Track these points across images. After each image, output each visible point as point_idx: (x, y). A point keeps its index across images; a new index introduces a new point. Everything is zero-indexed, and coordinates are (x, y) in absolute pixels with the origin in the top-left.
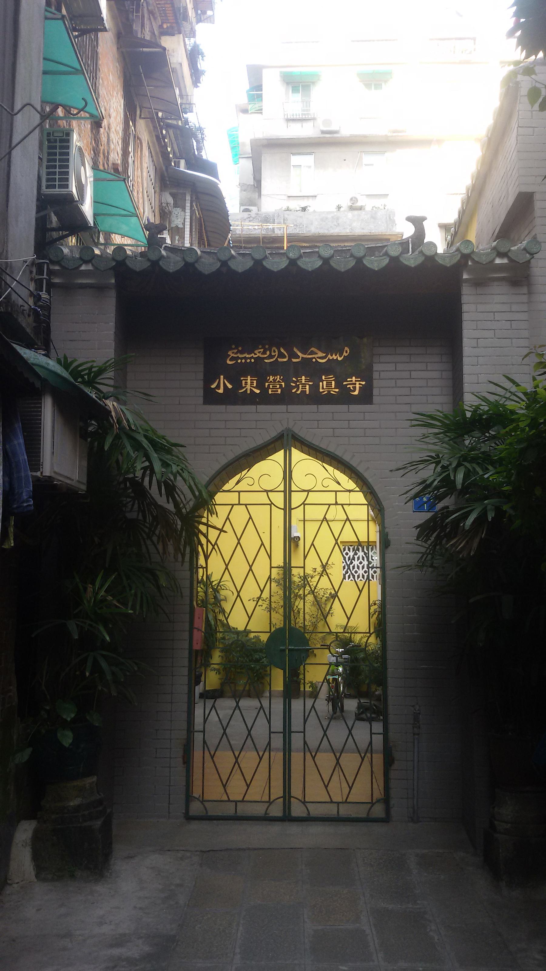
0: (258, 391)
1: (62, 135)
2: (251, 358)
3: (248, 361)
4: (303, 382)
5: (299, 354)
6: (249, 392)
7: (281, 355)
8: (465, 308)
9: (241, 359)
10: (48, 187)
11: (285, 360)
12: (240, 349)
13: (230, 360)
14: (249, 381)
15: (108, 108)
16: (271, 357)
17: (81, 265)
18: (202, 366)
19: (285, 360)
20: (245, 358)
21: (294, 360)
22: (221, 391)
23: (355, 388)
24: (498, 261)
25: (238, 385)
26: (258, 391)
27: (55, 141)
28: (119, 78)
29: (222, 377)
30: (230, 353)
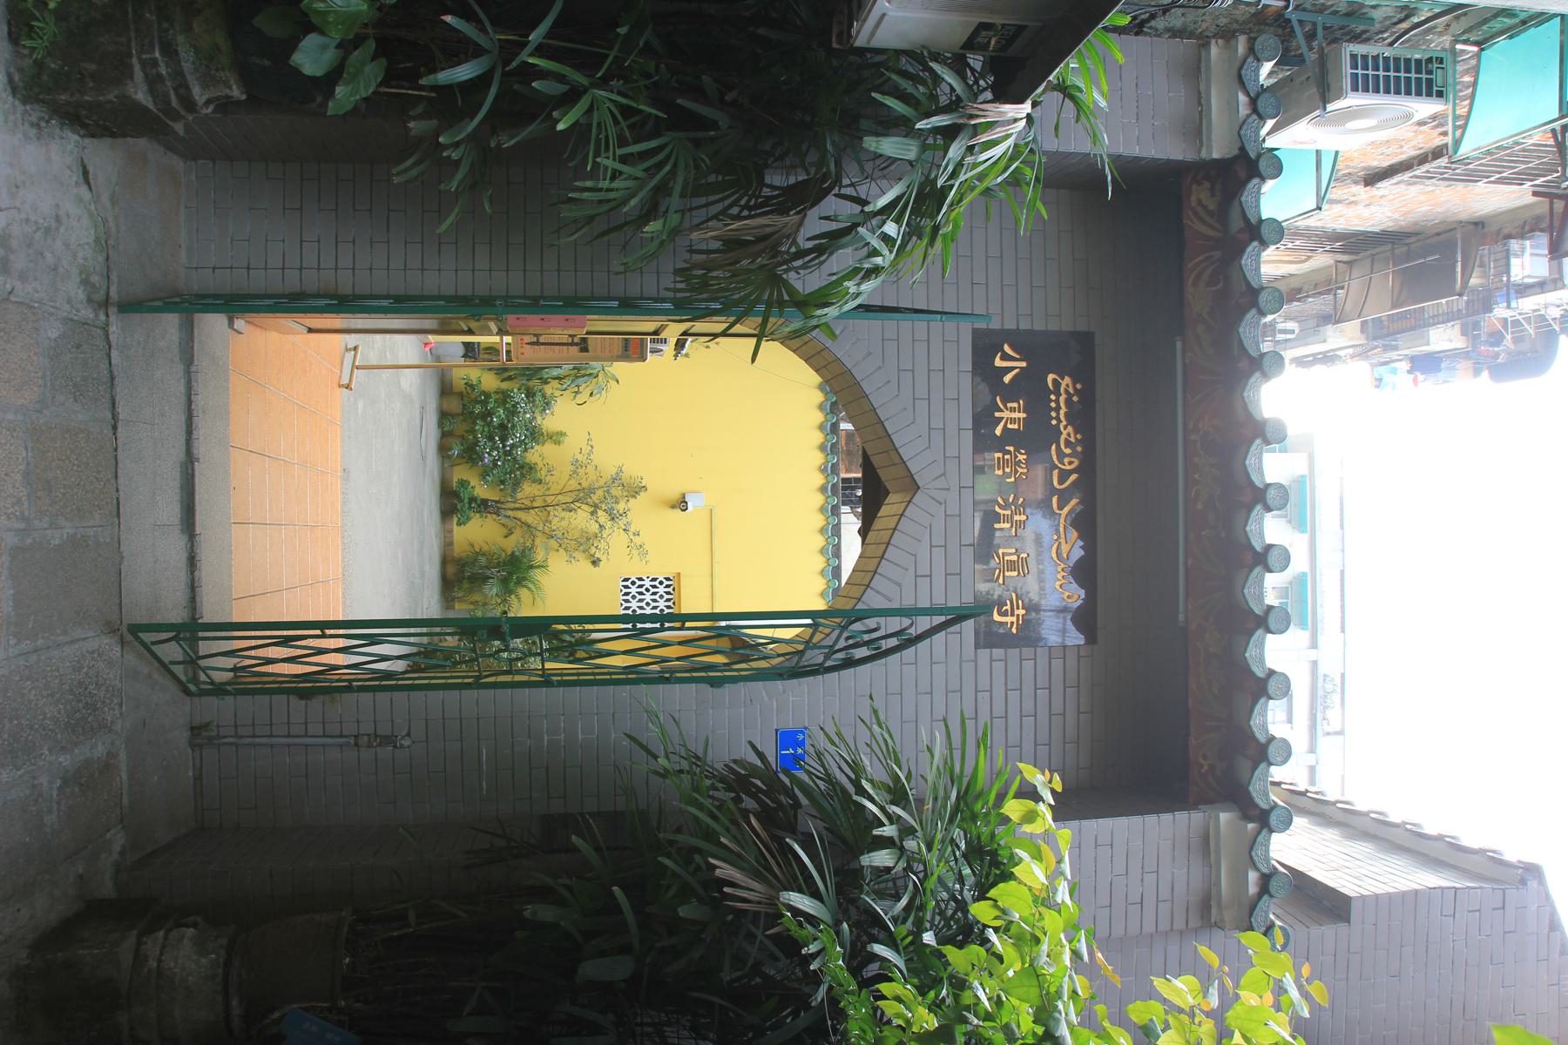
0: (998, 431)
1: (1439, 83)
2: (1058, 419)
3: (1053, 414)
4: (1017, 518)
5: (1066, 510)
6: (997, 414)
7: (1064, 476)
8: (1166, 817)
9: (1057, 401)
10: (1354, 57)
11: (1055, 483)
12: (1075, 399)
13: (1054, 380)
14: (1016, 415)
15: (1383, 202)
16: (1061, 455)
17: (1248, 94)
18: (1043, 328)
19: (1055, 483)
20: (1058, 409)
21: (1055, 500)
22: (998, 362)
23: (1005, 614)
24: (1253, 876)
25: (1010, 393)
26: (998, 431)
27: (1430, 72)
28: (1416, 223)
29: (1024, 364)
30: (1067, 380)
